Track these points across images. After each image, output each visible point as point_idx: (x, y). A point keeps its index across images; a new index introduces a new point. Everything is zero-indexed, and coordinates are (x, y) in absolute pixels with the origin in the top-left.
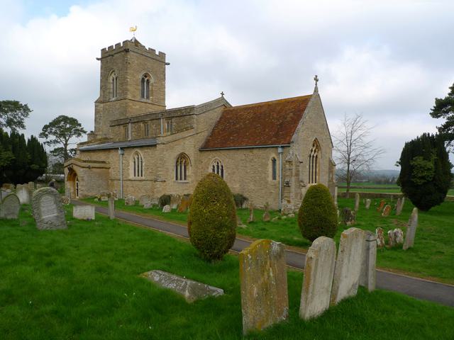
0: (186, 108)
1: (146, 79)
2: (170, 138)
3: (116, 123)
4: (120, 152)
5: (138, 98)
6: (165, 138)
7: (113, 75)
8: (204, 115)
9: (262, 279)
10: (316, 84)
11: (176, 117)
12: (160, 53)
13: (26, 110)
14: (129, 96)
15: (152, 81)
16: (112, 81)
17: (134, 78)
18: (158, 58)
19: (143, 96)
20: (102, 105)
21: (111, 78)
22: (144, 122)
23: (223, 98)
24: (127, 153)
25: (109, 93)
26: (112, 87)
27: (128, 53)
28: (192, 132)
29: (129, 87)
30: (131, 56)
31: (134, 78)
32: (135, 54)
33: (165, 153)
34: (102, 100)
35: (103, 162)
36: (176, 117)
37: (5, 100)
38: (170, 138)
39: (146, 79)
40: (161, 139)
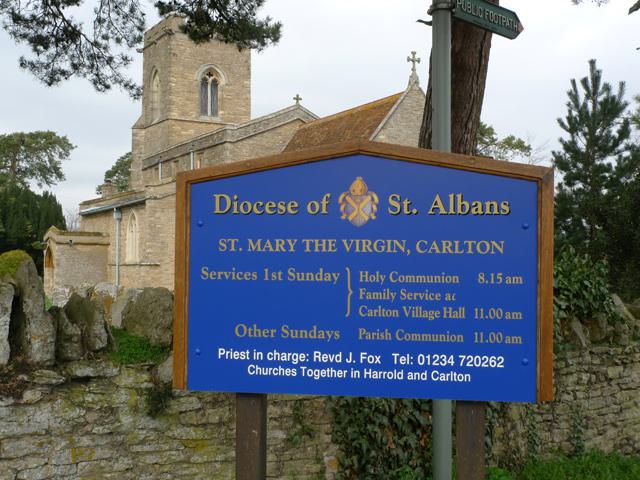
1: (210, 80)
4: (115, 215)
5: (193, 116)
9: (121, 398)
10: (413, 69)
11: (209, 148)
13: (65, 145)
14: (175, 114)
15: (222, 81)
19: (204, 111)
20: (143, 132)
23: (298, 107)
24: (126, 217)
33: (157, 215)
34: (143, 123)
35: (98, 234)
36: (209, 148)
37: (33, 131)
39: (210, 80)
40: (152, 189)
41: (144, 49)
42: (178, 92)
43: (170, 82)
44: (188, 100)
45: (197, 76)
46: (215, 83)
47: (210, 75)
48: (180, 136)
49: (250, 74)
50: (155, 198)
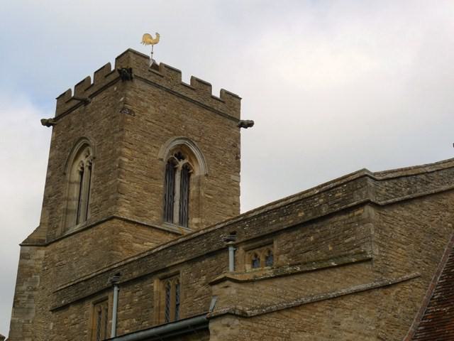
0: (327, 190)
2: (269, 294)
3: (73, 296)
5: (154, 218)
6: (248, 289)
7: (82, 158)
8: (403, 212)
12: (222, 92)
14: (125, 211)
15: (199, 169)
16: (76, 177)
17: (143, 156)
18: (220, 107)
19: (168, 216)
20: (42, 252)
21: (77, 168)
22: (166, 274)
25: (67, 211)
26: (76, 195)
27: (129, 84)
28: (360, 279)
29: (124, 181)
30: (137, 92)
31: (143, 156)
32: (147, 87)
38: (269, 294)
39: (181, 164)
40: (233, 290)
41: (56, 119)
42: (131, 174)
43: (121, 154)
44: (146, 189)
45: (163, 153)
46: (187, 172)
47: (180, 157)
48: (130, 249)
49: (239, 166)
50: (243, 316)
